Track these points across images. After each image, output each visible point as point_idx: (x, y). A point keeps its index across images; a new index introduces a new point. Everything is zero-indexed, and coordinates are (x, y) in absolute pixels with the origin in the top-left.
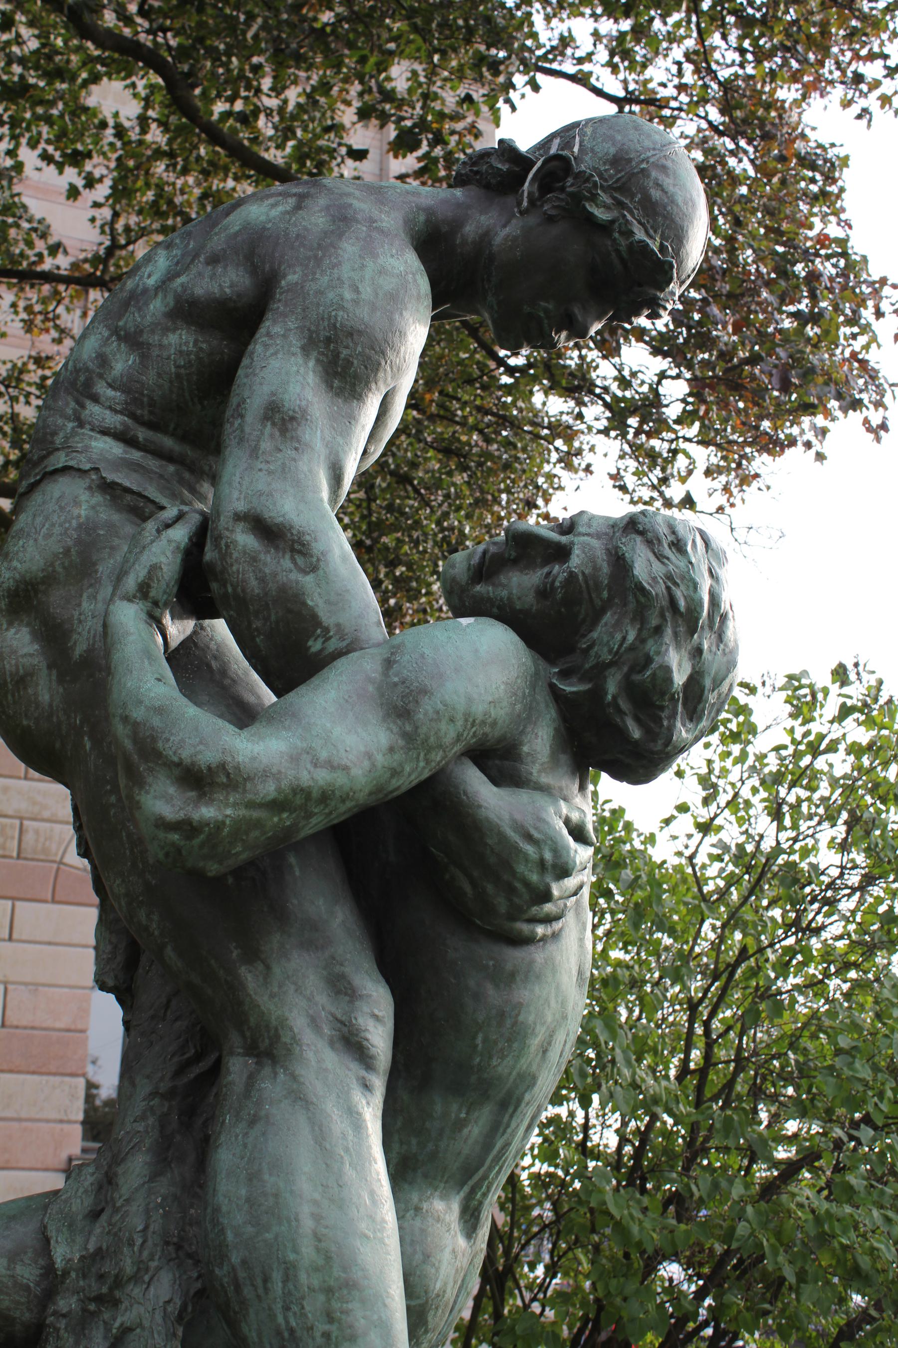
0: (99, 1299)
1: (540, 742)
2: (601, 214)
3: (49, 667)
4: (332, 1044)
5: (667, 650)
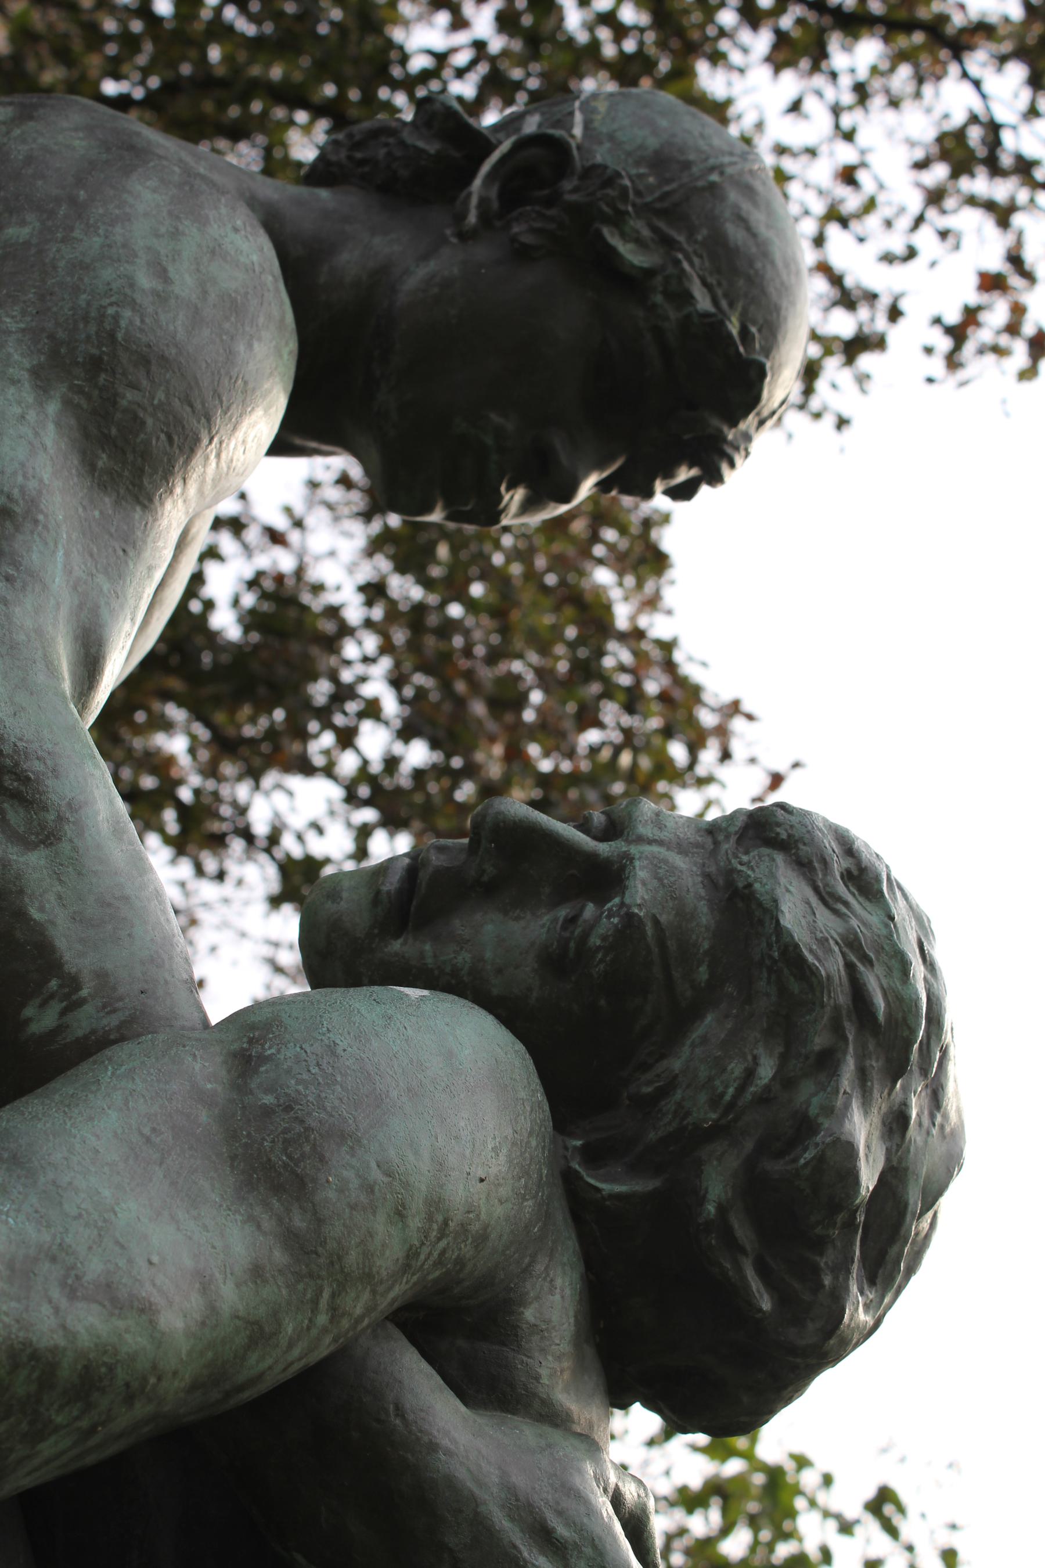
1: (553, 1304)
5: (847, 1106)
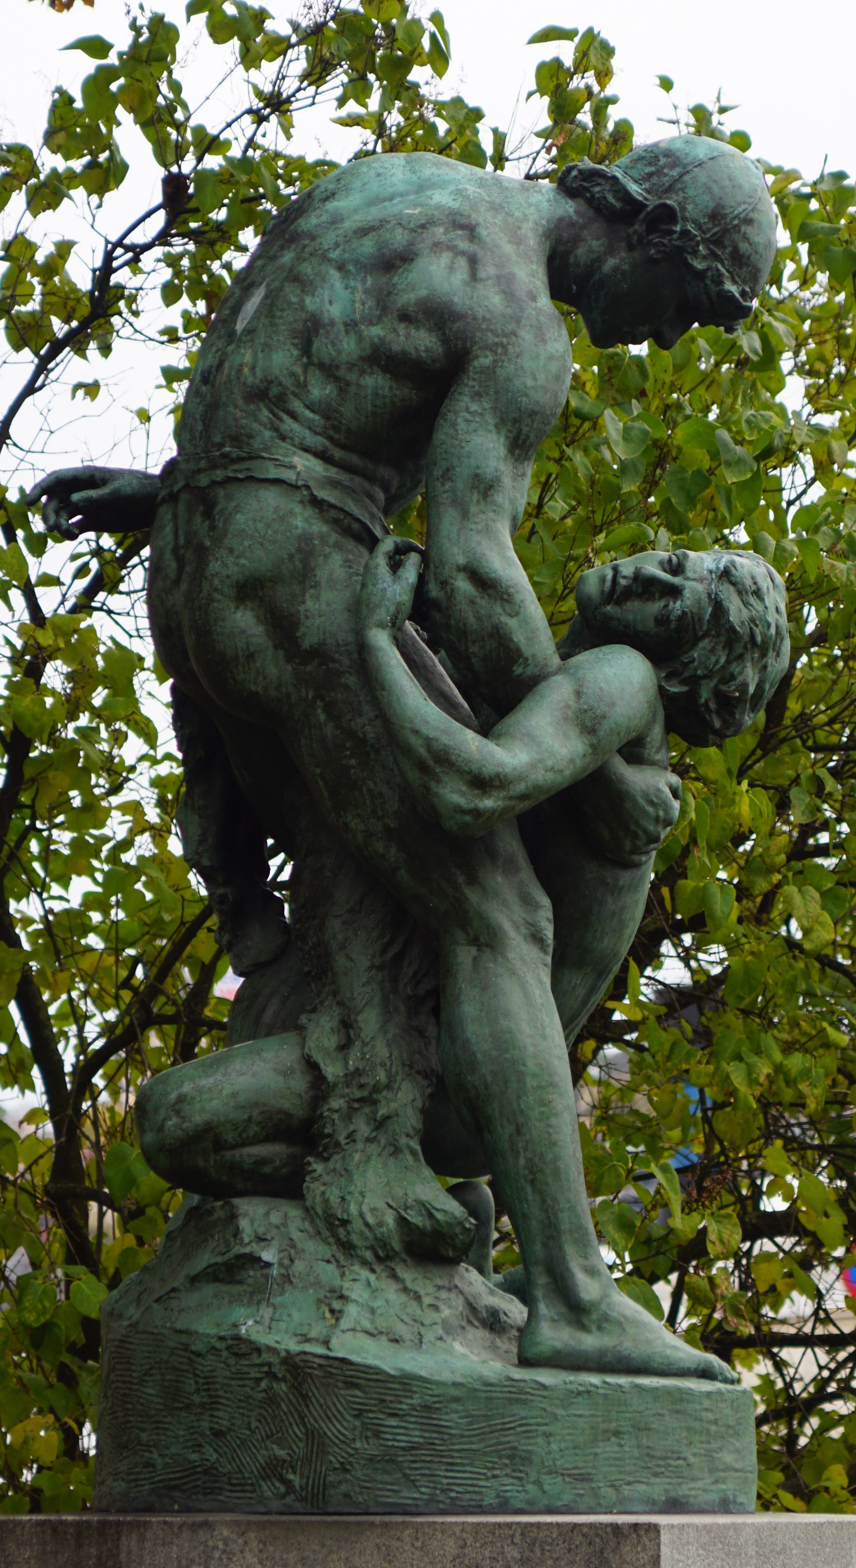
0: (361, 1100)
2: (699, 265)
3: (276, 647)
4: (525, 938)
